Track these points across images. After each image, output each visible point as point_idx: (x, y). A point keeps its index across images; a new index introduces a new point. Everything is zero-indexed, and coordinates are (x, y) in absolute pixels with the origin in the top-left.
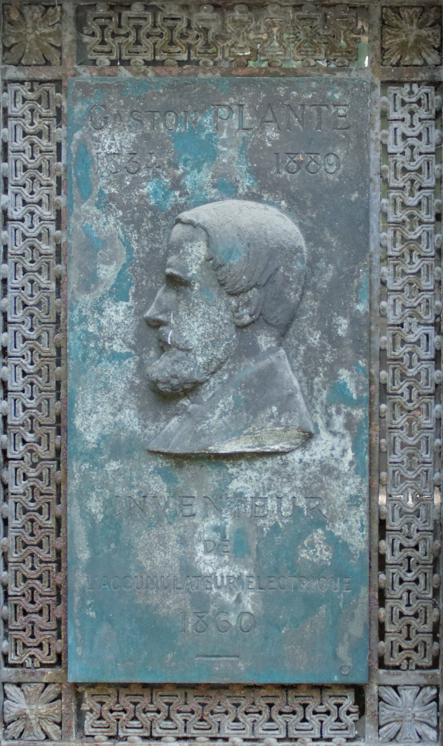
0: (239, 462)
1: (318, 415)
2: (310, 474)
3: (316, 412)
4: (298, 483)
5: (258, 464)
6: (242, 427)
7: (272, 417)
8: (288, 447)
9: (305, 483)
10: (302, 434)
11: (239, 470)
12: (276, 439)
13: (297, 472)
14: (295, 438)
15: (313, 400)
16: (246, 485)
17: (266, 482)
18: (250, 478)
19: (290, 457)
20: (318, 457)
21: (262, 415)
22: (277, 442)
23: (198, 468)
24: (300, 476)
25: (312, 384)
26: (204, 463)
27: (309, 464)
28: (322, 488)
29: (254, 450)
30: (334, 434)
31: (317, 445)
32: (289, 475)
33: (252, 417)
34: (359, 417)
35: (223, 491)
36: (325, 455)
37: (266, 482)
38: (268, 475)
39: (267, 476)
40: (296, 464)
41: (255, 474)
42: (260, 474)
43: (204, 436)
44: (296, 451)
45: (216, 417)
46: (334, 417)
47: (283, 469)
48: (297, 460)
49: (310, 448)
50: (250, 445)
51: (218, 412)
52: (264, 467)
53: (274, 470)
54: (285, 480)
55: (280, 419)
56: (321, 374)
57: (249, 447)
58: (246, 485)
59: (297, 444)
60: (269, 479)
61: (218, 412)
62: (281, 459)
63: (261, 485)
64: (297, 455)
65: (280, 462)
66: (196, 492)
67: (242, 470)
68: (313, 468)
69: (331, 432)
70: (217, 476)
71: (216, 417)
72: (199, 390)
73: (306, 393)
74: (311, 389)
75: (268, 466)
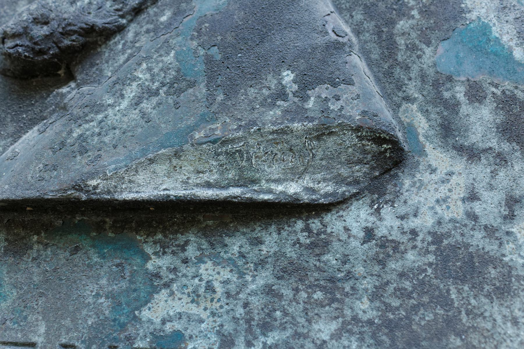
0: (181, 239)
1: (415, 107)
2: (402, 275)
3: (408, 99)
4: (364, 308)
5: (236, 244)
6: (191, 121)
7: (282, 95)
8: (330, 189)
9: (388, 307)
10: (370, 146)
11: (178, 263)
12: (291, 161)
13: (360, 269)
14: (350, 162)
15: (398, 70)
16: (194, 309)
17: (256, 302)
18: (210, 288)
19: (334, 223)
20: (425, 221)
21: (252, 91)
22: (296, 174)
23: (63, 255)
24: (368, 284)
25: (391, 36)
26: (85, 242)
27: (396, 245)
28: (451, 324)
29: (224, 194)
30: (472, 154)
31: (421, 186)
32: (332, 280)
33: (220, 98)
34: (427, 297)
35: (123, 327)
36: (447, 216)
37: (256, 302)
38: (265, 277)
39: (261, 282)
40: (354, 243)
41: (226, 274)
42: (241, 275)
43: (83, 151)
44: (355, 205)
45: (124, 104)
46: (465, 109)
47: (313, 261)
48: (357, 231)
49: (397, 195)
50: (213, 178)
51: (131, 91)
52: (253, 255)
53: (284, 263)
54: (318, 295)
55: (305, 98)
56: (415, 12)
57: (208, 185)
58: (194, 309)
59: (356, 182)
60: (269, 290)
61: (131, 91)
62: (307, 229)
63: (240, 311)
64: (358, 216)
65: (303, 238)
66: (42, 329)
67: (185, 261)
68: (411, 256)
69: (460, 149)
70: (113, 278)
71: (124, 104)
72: (100, 54)
73: (375, 56)
74: (389, 47)
75: (264, 249)
